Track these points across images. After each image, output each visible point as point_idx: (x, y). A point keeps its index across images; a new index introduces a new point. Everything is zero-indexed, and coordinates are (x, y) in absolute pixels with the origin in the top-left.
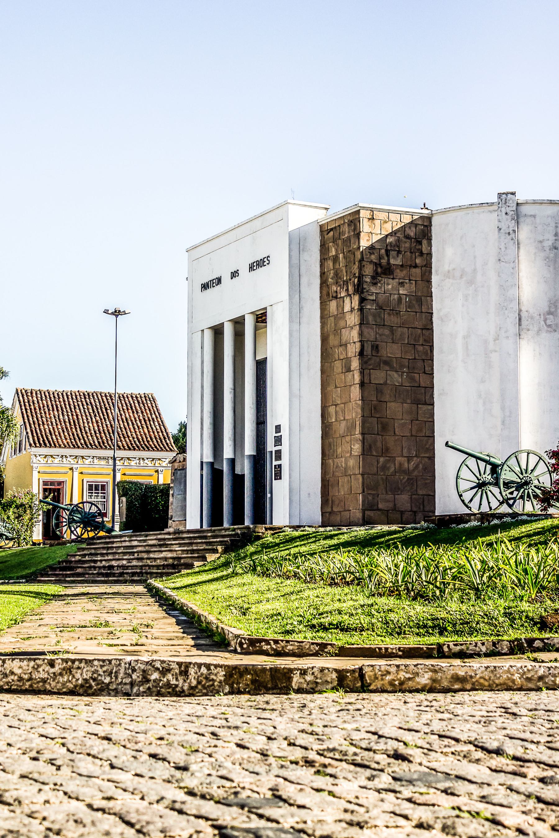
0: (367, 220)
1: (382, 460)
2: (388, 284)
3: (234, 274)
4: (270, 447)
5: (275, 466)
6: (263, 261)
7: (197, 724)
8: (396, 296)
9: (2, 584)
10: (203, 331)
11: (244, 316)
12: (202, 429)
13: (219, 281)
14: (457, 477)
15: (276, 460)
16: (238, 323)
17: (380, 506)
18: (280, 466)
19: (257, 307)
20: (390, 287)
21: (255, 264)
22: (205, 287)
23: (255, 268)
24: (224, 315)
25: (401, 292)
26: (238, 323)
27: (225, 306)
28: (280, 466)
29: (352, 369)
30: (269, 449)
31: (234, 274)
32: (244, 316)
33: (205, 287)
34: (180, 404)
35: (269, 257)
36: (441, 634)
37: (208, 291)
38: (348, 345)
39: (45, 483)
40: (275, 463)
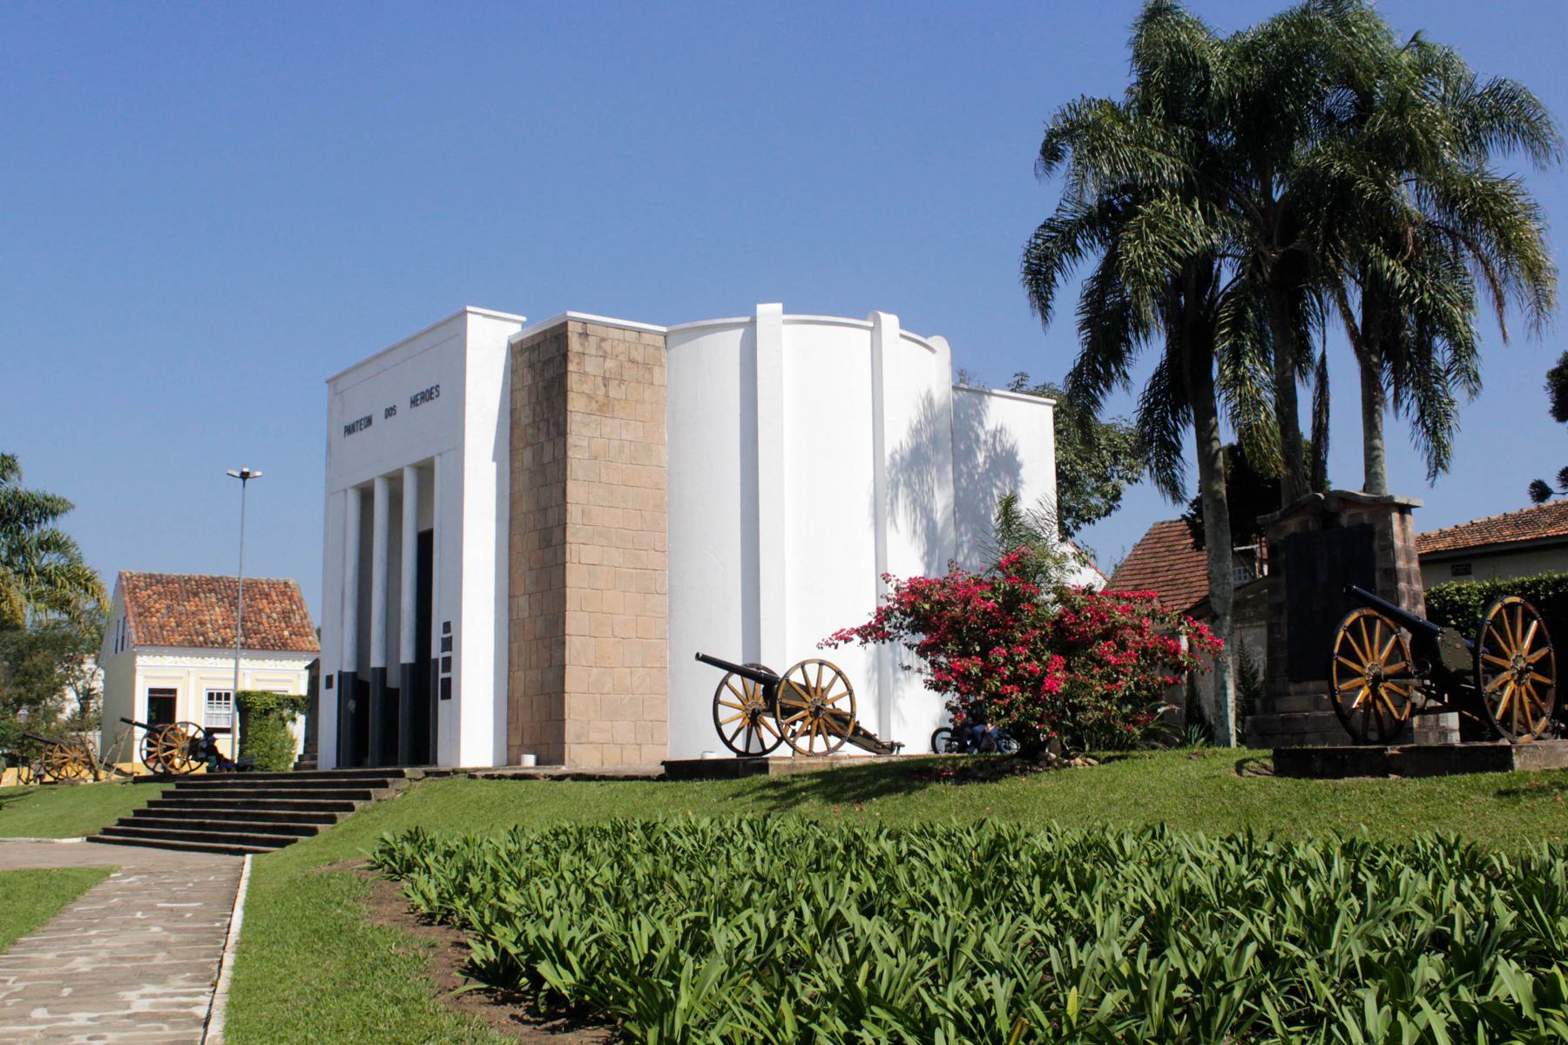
1: (595, 671)
3: (390, 412)
4: (436, 652)
6: (430, 392)
7: (1352, 928)
8: (616, 443)
9: (1562, 581)
11: (372, 481)
12: (342, 625)
13: (369, 421)
14: (716, 702)
16: (394, 482)
17: (592, 737)
18: (449, 680)
19: (418, 456)
22: (349, 430)
24: (373, 471)
26: (394, 482)
27: (374, 458)
30: (434, 656)
31: (390, 412)
32: (372, 481)
33: (349, 430)
34: (321, 596)
36: (813, 893)
37: (355, 436)
39: (151, 691)
40: (441, 675)
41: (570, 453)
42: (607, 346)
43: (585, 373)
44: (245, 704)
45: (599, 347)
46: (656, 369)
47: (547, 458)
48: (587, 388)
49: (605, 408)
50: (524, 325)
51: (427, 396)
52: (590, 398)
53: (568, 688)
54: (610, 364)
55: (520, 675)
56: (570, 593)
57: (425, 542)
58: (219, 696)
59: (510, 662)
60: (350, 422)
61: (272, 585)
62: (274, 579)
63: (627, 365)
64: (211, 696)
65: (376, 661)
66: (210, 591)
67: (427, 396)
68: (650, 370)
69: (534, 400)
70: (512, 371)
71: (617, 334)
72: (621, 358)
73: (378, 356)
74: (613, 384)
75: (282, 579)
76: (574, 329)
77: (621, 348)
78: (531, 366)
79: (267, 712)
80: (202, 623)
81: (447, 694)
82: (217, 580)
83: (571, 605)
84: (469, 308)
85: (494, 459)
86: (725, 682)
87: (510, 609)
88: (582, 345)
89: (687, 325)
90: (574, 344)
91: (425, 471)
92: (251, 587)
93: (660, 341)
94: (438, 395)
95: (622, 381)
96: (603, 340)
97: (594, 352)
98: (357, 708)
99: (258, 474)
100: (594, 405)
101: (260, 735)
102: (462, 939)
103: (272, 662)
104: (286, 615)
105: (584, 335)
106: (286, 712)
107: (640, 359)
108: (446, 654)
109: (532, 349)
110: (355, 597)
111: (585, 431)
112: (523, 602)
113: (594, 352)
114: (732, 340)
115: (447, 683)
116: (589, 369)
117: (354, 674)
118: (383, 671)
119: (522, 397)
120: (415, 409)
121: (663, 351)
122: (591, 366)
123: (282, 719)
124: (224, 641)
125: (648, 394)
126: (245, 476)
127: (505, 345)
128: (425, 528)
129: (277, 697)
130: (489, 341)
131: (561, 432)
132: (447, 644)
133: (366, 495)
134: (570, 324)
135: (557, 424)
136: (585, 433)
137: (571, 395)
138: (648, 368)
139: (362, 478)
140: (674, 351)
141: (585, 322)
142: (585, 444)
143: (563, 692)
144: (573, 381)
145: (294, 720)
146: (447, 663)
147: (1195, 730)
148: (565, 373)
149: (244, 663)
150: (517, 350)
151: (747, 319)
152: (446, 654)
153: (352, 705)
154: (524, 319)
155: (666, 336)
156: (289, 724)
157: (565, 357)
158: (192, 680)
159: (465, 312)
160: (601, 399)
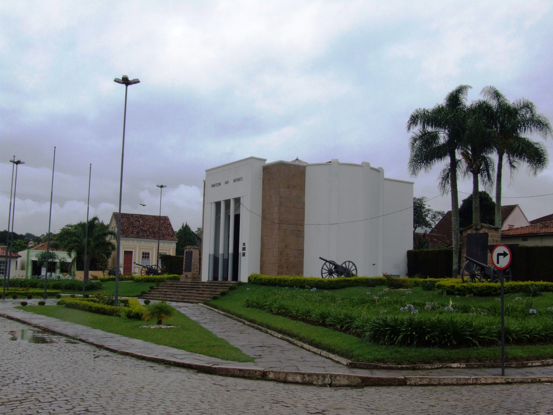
3: (227, 182)
13: (234, 181)
14: (323, 268)
16: (228, 202)
24: (222, 198)
26: (228, 202)
31: (227, 182)
51: (239, 180)
57: (237, 218)
60: (213, 184)
67: (239, 180)
86: (325, 264)
102: (310, 378)
128: (237, 213)
133: (218, 204)
147: (163, 315)
152: (244, 251)
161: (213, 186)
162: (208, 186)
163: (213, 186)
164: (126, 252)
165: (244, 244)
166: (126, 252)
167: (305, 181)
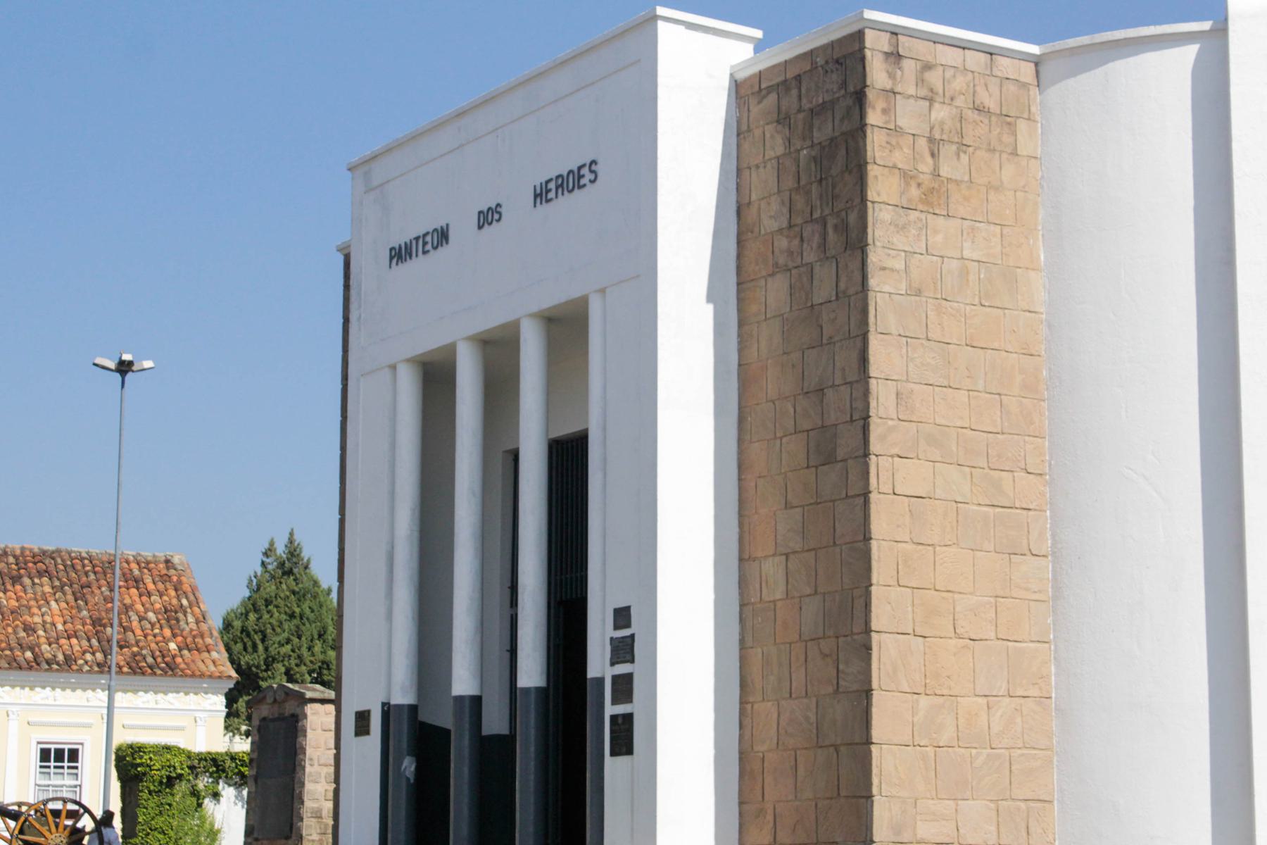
0: (881, 57)
1: (924, 702)
2: (936, 232)
3: (489, 217)
4: (598, 664)
5: (614, 718)
8: (955, 264)
10: (393, 368)
11: (451, 350)
13: (443, 236)
15: (615, 701)
16: (499, 351)
18: (629, 718)
19: (553, 296)
20: (939, 238)
21: (552, 185)
23: (551, 195)
25: (966, 254)
26: (499, 351)
27: (444, 308)
28: (629, 718)
29: (841, 453)
30: (592, 673)
31: (489, 217)
32: (451, 350)
35: (594, 162)
38: (830, 393)
41: (873, 282)
42: (934, 78)
43: (897, 130)
44: (131, 767)
45: (920, 81)
46: (1022, 126)
47: (823, 290)
48: (899, 158)
49: (934, 196)
50: (759, 46)
51: (570, 182)
52: (907, 177)
53: (876, 734)
54: (940, 113)
55: (765, 709)
56: (879, 550)
57: (569, 459)
58: (59, 755)
59: (743, 685)
60: (400, 239)
61: (145, 565)
62: (148, 554)
63: (970, 115)
64: (45, 755)
65: (463, 682)
66: (40, 574)
67: (570, 182)
68: (1012, 127)
69: (790, 183)
70: (740, 132)
71: (950, 56)
72: (959, 102)
73: (461, 114)
74: (948, 151)
75: (161, 555)
76: (875, 43)
77: (959, 83)
78: (782, 119)
79: (170, 782)
80: (30, 629)
81: (624, 740)
82: (52, 555)
83: (880, 574)
84: (661, 11)
85: (710, 298)
87: (743, 583)
88: (891, 76)
89: (1085, 40)
90: (877, 73)
91: (566, 328)
92: (104, 567)
93: (1027, 72)
94: (597, 178)
95: (962, 146)
96: (928, 67)
97: (911, 90)
98: (418, 769)
99: (148, 364)
100: (914, 192)
101: (159, 822)
103: (150, 696)
104: (171, 616)
105: (895, 57)
106: (203, 783)
107: (991, 103)
108: (622, 669)
109: (783, 87)
110: (415, 564)
111: (899, 241)
112: (772, 569)
113: (911, 90)
114: (1168, 73)
115: (624, 726)
116: (903, 122)
117: (413, 709)
118: (477, 701)
119: (763, 181)
120: (543, 209)
121: (1034, 91)
122: (908, 115)
123: (195, 793)
124: (69, 661)
125: (1008, 173)
126: (124, 368)
127: (725, 82)
128: (566, 429)
129: (189, 755)
130: (698, 75)
131: (855, 241)
132: (623, 650)
133: (436, 378)
134: (870, 36)
135: (843, 228)
136: (901, 247)
137: (872, 170)
138: (1007, 121)
139: (428, 342)
140: (1054, 93)
141: (894, 33)
142: (899, 265)
143: (868, 742)
144: (876, 143)
145: (216, 795)
146: (624, 687)
148: (862, 127)
149: (121, 699)
150: (745, 92)
151: (1206, 25)
152: (622, 669)
153: (409, 766)
154: (758, 34)
155: (1037, 62)
156: (208, 803)
157: (860, 98)
158: (14, 726)
159: (655, 18)
160: (925, 179)
161: (400, 254)
162: (370, 265)
163: (400, 254)
164: (367, 733)
165: (622, 616)
166: (367, 733)
167: (713, 247)
